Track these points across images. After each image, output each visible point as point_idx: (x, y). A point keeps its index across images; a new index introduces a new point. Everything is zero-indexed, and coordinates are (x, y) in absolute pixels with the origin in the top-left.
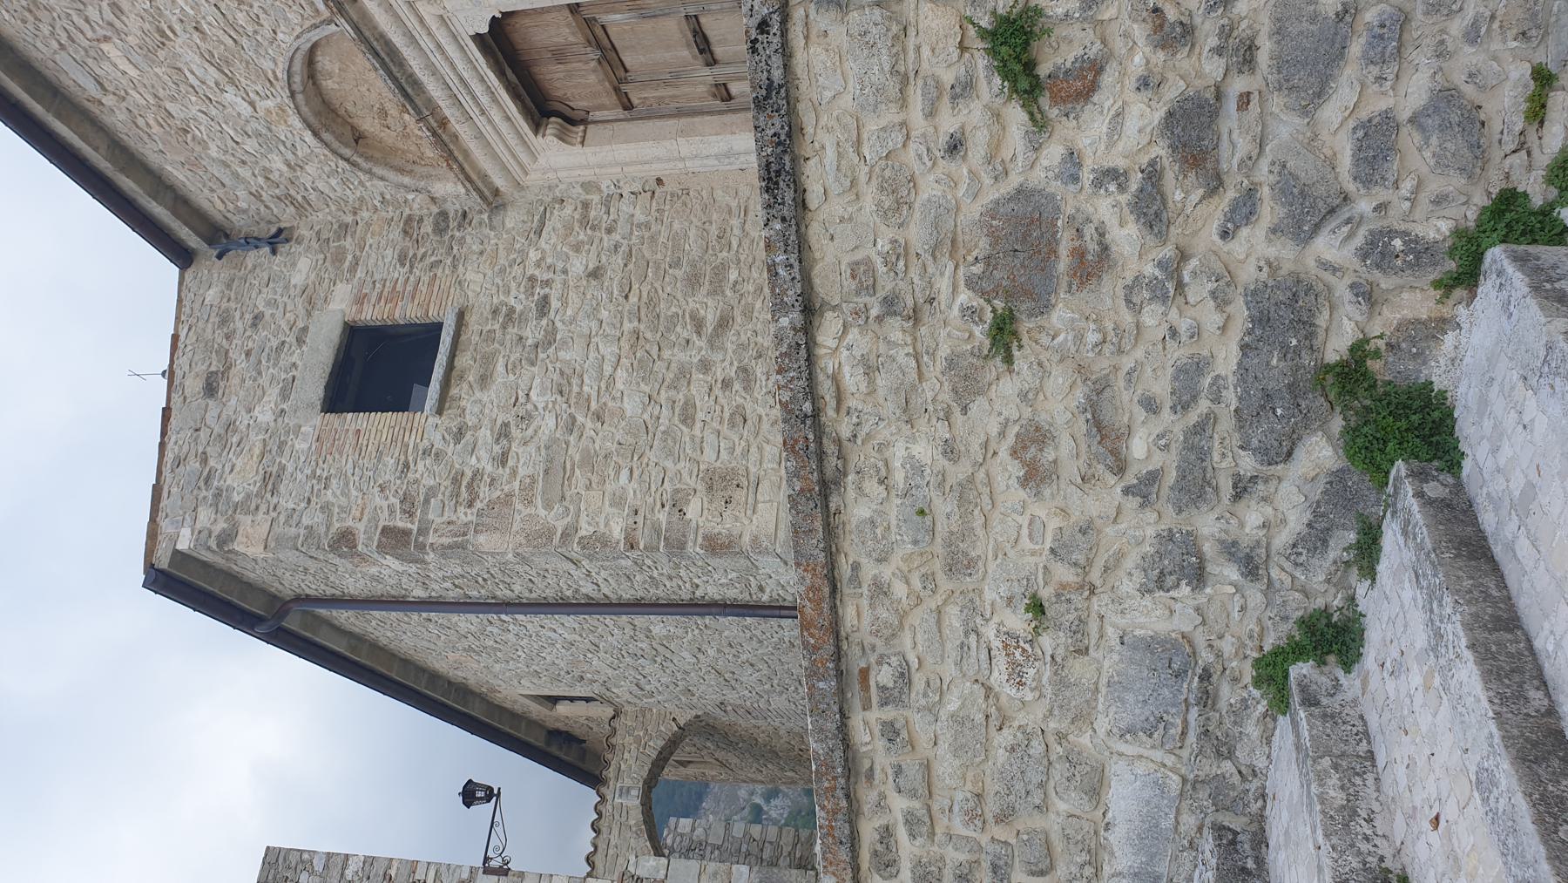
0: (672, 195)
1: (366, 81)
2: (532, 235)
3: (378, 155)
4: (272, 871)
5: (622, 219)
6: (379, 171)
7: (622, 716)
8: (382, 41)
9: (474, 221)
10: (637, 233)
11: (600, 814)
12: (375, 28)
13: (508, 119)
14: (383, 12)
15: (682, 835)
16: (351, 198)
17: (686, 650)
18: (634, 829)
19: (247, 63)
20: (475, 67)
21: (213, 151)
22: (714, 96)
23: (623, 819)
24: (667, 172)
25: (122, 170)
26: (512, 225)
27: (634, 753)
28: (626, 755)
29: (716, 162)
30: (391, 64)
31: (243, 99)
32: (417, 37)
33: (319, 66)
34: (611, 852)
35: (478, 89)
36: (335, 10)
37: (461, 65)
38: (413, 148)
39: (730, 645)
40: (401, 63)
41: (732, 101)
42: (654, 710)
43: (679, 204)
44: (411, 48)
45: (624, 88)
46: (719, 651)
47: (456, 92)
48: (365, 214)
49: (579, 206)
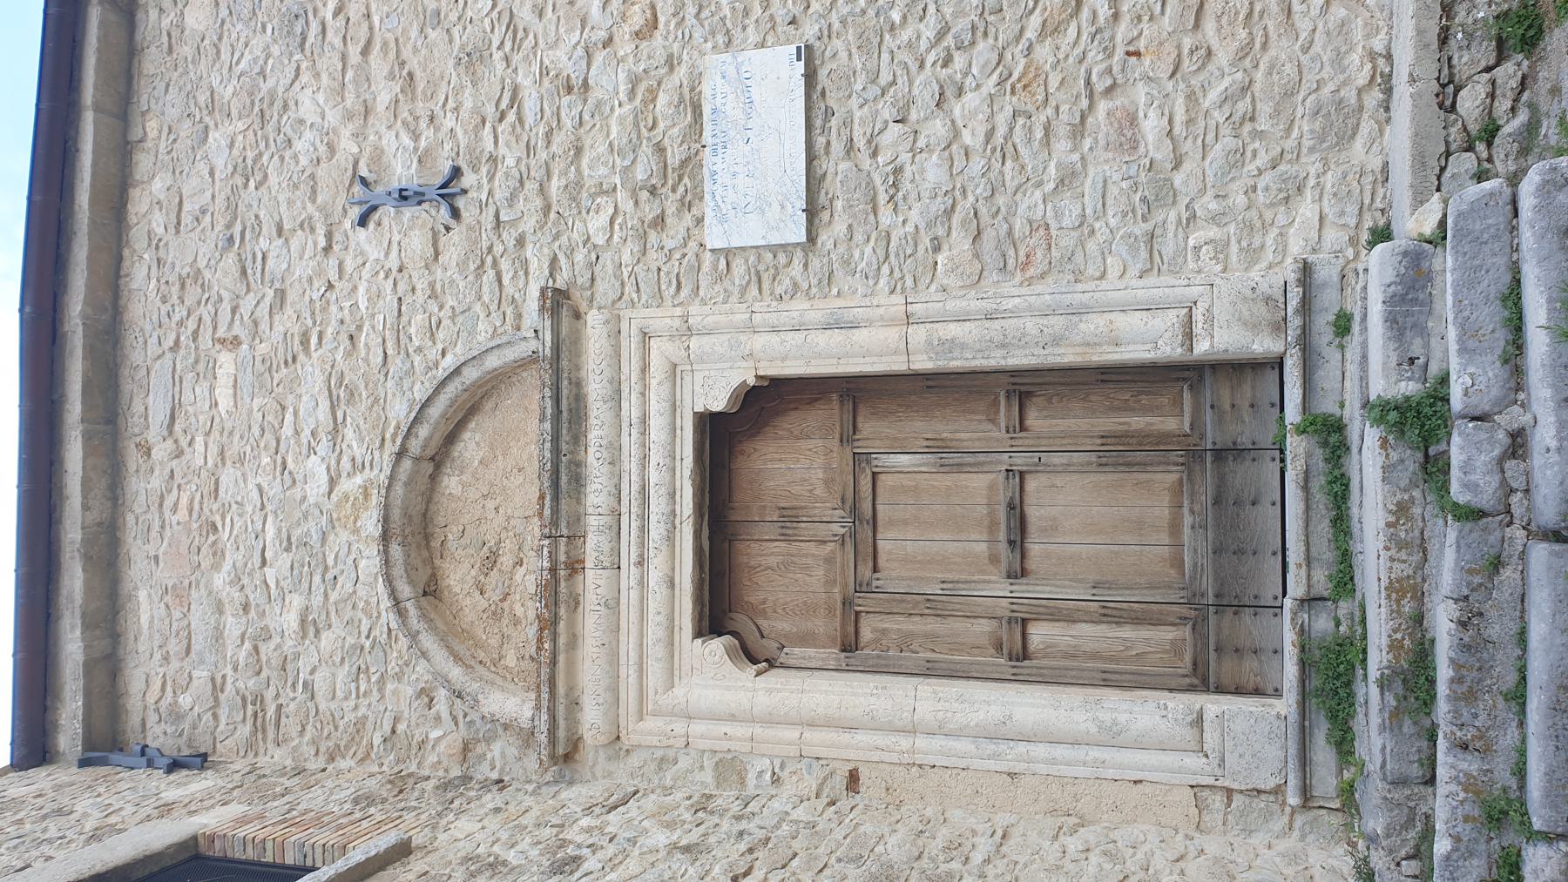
3: (439, 624)
6: (428, 641)
12: (578, 368)
13: (671, 584)
19: (376, 400)
20: (674, 469)
21: (220, 580)
22: (999, 647)
24: (876, 756)
25: (87, 558)
30: (565, 425)
31: (328, 469)
32: (625, 394)
33: (458, 450)
35: (658, 506)
38: (494, 641)
40: (578, 438)
41: (1026, 663)
44: (609, 404)
45: (863, 603)
47: (624, 510)
48: (344, 764)
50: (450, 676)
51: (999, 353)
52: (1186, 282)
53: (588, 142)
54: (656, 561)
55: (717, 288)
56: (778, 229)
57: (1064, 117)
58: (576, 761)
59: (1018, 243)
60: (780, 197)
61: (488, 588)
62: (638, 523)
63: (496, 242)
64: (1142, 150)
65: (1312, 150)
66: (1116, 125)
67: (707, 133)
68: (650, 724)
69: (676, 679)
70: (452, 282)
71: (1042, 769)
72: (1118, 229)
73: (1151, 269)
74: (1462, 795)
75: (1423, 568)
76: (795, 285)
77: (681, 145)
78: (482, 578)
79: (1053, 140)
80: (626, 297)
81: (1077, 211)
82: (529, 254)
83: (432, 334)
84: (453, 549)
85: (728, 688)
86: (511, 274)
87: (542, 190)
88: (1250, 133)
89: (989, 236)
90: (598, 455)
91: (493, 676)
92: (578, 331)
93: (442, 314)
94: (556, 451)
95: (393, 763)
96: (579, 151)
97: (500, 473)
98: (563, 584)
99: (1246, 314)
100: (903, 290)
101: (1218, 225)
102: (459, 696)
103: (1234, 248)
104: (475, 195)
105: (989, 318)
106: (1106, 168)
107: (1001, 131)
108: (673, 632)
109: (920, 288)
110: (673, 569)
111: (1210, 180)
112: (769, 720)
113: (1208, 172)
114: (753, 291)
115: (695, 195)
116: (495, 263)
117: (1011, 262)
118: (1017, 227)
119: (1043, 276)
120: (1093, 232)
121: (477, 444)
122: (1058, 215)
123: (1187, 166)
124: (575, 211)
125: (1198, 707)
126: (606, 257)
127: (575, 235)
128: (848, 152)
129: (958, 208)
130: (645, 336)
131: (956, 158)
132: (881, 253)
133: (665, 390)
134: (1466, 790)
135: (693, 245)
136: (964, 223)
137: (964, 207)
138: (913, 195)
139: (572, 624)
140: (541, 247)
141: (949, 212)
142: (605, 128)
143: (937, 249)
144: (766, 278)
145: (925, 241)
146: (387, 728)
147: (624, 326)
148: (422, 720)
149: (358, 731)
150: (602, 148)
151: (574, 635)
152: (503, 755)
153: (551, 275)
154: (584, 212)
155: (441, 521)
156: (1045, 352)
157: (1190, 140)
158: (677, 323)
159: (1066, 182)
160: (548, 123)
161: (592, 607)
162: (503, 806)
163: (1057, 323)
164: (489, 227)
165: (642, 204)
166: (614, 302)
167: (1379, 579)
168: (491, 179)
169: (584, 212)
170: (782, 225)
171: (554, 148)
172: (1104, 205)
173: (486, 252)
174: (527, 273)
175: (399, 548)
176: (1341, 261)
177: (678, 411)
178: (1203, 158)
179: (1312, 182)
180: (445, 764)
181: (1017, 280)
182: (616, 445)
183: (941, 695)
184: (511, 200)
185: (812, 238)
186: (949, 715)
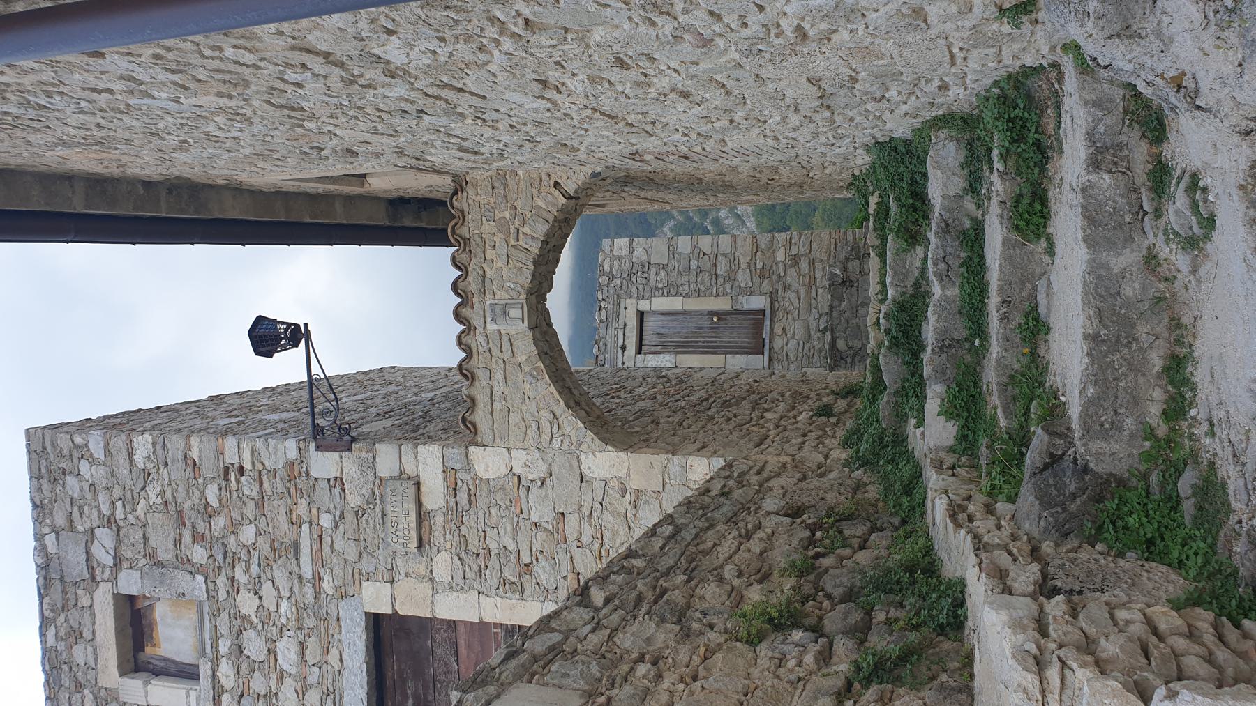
4: (44, 463)
7: (469, 188)
11: (469, 352)
15: (620, 258)
17: (508, 88)
18: (526, 369)
23: (507, 355)
27: (502, 248)
28: (490, 254)
34: (497, 405)
39: (620, 63)
42: (520, 173)
46: (593, 80)
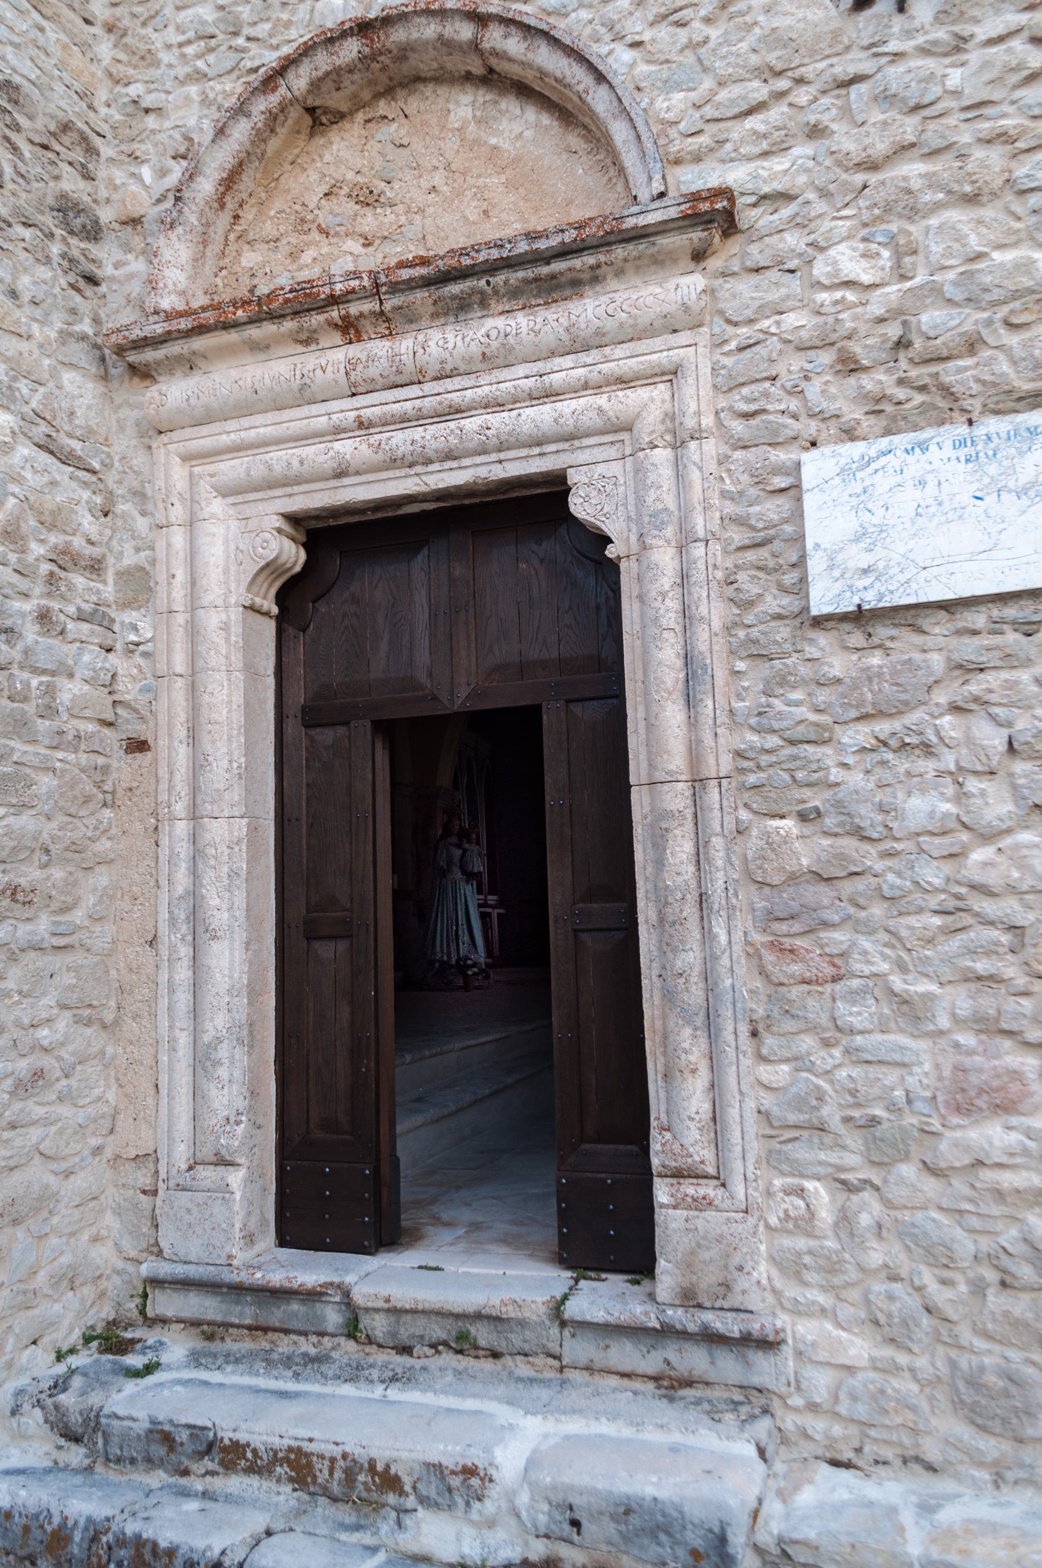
0: (105, 770)
1: (459, 194)
2: (43, 428)
3: (273, 144)
5: (66, 648)
6: (241, 131)
8: (585, 276)
9: (78, 298)
10: (34, 683)
12: (620, 273)
13: (340, 473)
14: (667, 308)
16: (158, 40)
20: (485, 452)
24: (163, 772)
26: (66, 383)
29: (180, 890)
33: (510, 104)
36: (705, 206)
37: (498, 421)
38: (269, 229)
43: (89, 788)
44: (565, 337)
47: (429, 387)
48: (105, 49)
49: (96, 551)
50: (200, 179)
51: (653, 915)
52: (750, 1176)
53: (988, 213)
54: (364, 447)
55: (745, 478)
56: (831, 568)
57: (1011, 1005)
58: (131, 379)
59: (813, 936)
60: (881, 565)
61: (332, 204)
62: (410, 412)
63: (812, 89)
64: (955, 1120)
65: (953, 1365)
66: (996, 1083)
67: (994, 425)
68: (179, 474)
69: (231, 500)
70: (749, 27)
71: (163, 977)
72: (831, 1082)
73: (771, 1126)
74: (49, 1529)
75: (324, 1495)
76: (751, 604)
77: (978, 380)
78: (345, 190)
79: (973, 986)
80: (730, 330)
81: (856, 1022)
82: (796, 151)
83: (665, 17)
84: (379, 136)
85: (226, 571)
86: (761, 128)
87: (904, 149)
88: (982, 1279)
89: (823, 894)
90: (494, 334)
91: (219, 238)
92: (675, 261)
93: (696, 24)
94: (492, 268)
95: (111, 121)
96: (972, 199)
97: (481, 182)
98: (321, 318)
99: (706, 1255)
100: (742, 771)
101: (836, 1224)
102: (178, 199)
103: (801, 1243)
104: (896, 29)
105: (702, 899)
106: (927, 1067)
107: (989, 907)
108: (284, 485)
109: (746, 795)
110: (357, 473)
111: (906, 1216)
112: (193, 631)
113: (919, 1215)
114: (738, 536)
115: (894, 418)
116: (781, 95)
117: (783, 927)
118: (837, 935)
119: (763, 973)
120: (827, 1044)
121: (520, 135)
122: (852, 998)
123: (930, 1186)
124: (866, 216)
125: (239, 1161)
126: (794, 285)
127: (827, 224)
128: (960, 667)
129: (867, 847)
130: (672, 374)
131: (946, 840)
132: (799, 732)
133: (591, 420)
134: (53, 1532)
135: (811, 428)
136: (841, 857)
137: (870, 857)
138: (887, 776)
139: (280, 340)
140: (807, 170)
141: (859, 834)
142: (1013, 238)
143: (803, 817)
144: (764, 553)
145: (815, 800)
146: (148, 101)
147: (684, 338)
148: (160, 147)
149: (143, 58)
150: (974, 243)
151: (268, 347)
152: (131, 276)
153: (764, 197)
154: (864, 232)
155: (413, 104)
156: (655, 979)
157: (967, 1191)
158: (690, 423)
159: (905, 1008)
160: (1023, 132)
161: (299, 366)
162: (26, 297)
163: (695, 995)
164: (837, 70)
165: (882, 329)
166: (721, 312)
167: (311, 1440)
168: (925, 51)
169: (864, 232)
170: (837, 573)
171: (979, 153)
172: (867, 1062)
173: (797, 74)
174: (765, 154)
175: (354, 54)
176: (783, 1390)
177: (566, 445)
178: (941, 1208)
179: (903, 1359)
180: (115, 197)
181: (758, 938)
182: (511, 359)
183: (237, 849)
184: (886, 98)
185: (819, 622)
186: (212, 862)
